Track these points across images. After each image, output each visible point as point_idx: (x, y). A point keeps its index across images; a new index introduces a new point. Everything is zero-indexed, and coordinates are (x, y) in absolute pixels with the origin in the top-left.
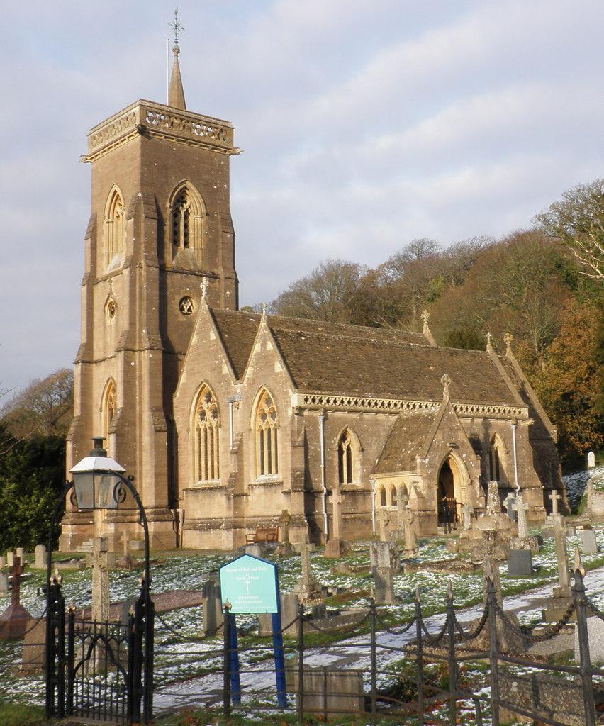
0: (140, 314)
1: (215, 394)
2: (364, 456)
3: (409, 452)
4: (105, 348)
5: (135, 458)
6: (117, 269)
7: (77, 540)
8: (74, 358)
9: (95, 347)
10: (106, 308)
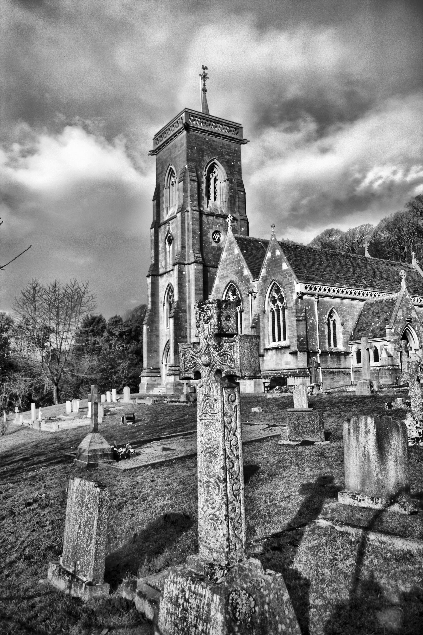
0: (188, 240)
1: (239, 290)
2: (344, 329)
3: (377, 325)
4: (166, 265)
5: (186, 333)
6: (173, 215)
7: (150, 387)
8: (147, 273)
9: (160, 266)
10: (167, 240)
